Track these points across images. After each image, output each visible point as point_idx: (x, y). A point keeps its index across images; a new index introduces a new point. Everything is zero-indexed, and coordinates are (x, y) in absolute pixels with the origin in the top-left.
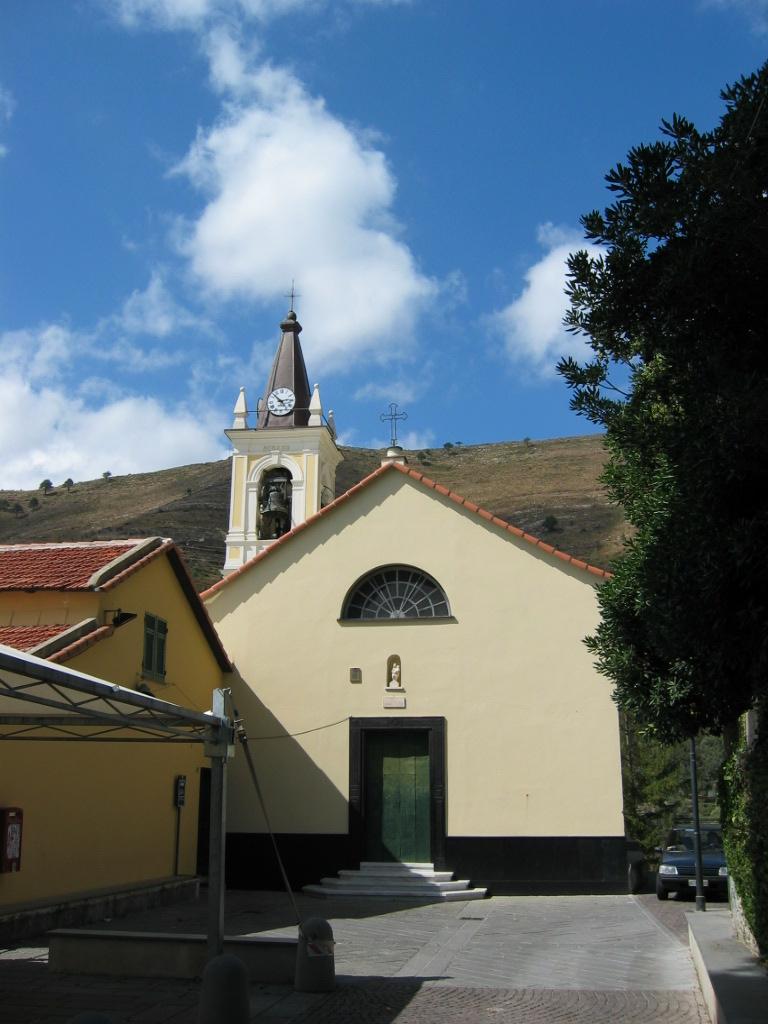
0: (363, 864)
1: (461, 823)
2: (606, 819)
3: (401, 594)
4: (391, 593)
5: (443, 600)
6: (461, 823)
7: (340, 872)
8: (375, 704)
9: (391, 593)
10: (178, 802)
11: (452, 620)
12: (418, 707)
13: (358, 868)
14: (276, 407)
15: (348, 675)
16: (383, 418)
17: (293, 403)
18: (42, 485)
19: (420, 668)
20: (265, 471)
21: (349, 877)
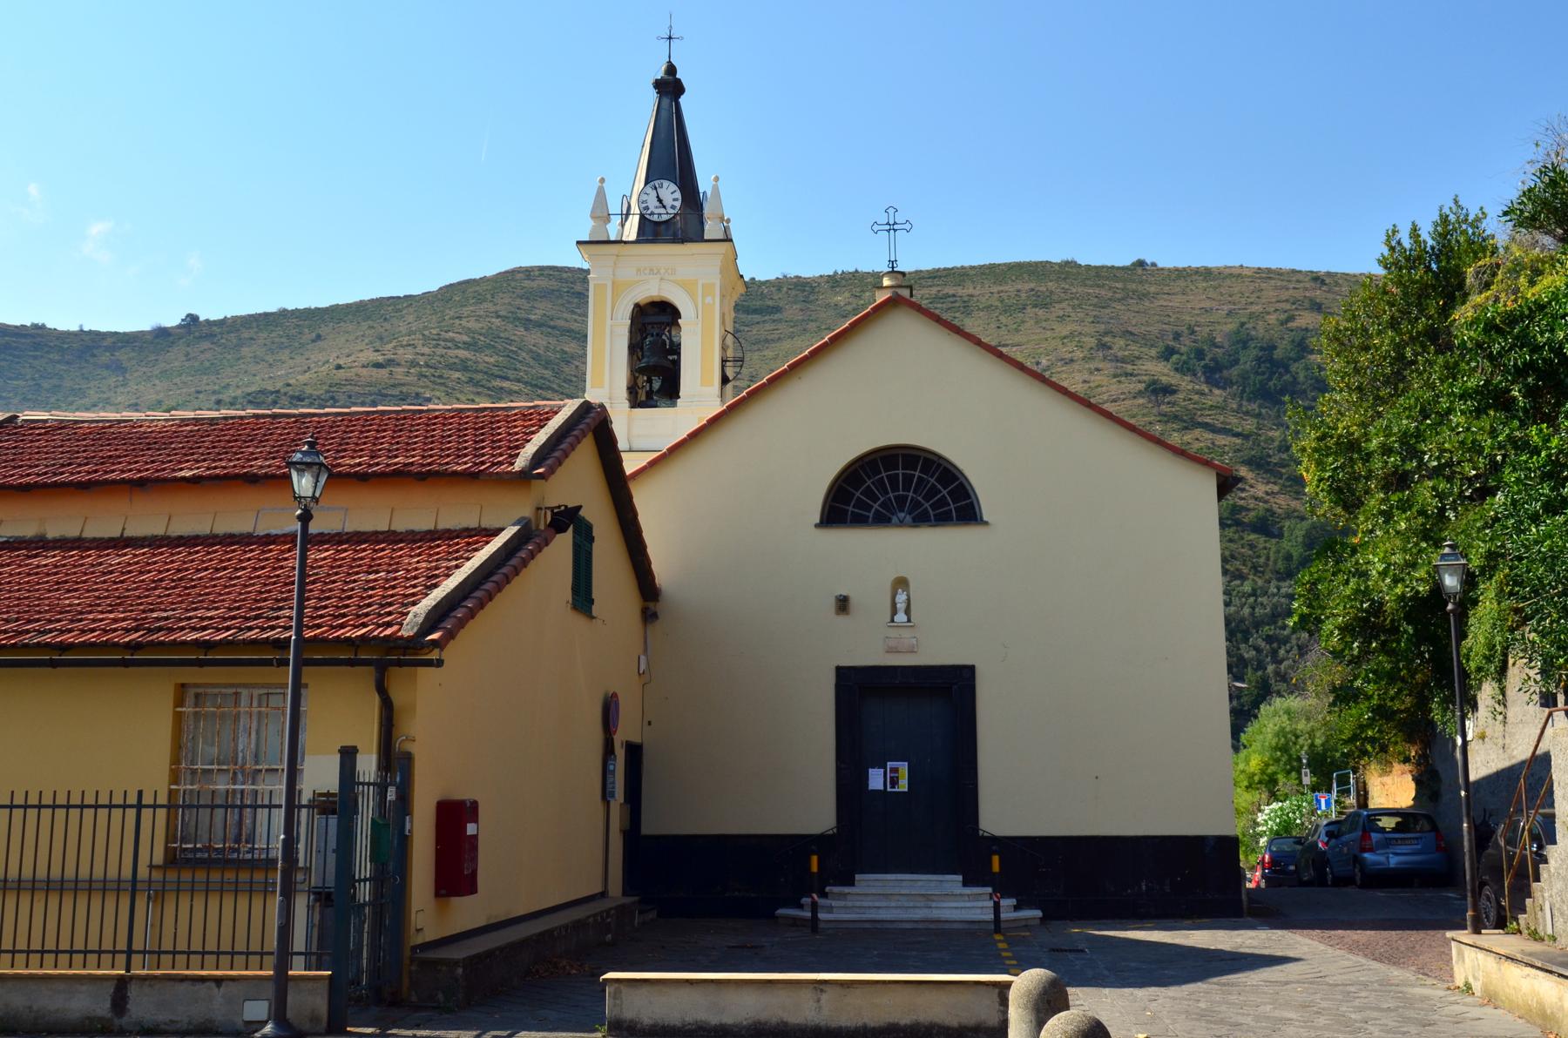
0: (858, 877)
1: (1001, 813)
2: (647, 829)
3: (907, 489)
4: (899, 487)
5: (969, 497)
6: (1001, 813)
7: (828, 889)
8: (869, 647)
9: (899, 487)
10: (606, 795)
11: (986, 523)
12: (936, 651)
13: (851, 883)
14: (652, 209)
15: (831, 603)
16: (907, 226)
17: (678, 204)
18: (1402, 261)
19: (924, 594)
20: (637, 305)
21: (843, 896)
